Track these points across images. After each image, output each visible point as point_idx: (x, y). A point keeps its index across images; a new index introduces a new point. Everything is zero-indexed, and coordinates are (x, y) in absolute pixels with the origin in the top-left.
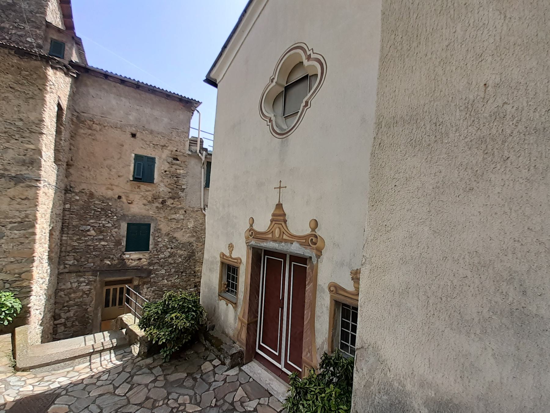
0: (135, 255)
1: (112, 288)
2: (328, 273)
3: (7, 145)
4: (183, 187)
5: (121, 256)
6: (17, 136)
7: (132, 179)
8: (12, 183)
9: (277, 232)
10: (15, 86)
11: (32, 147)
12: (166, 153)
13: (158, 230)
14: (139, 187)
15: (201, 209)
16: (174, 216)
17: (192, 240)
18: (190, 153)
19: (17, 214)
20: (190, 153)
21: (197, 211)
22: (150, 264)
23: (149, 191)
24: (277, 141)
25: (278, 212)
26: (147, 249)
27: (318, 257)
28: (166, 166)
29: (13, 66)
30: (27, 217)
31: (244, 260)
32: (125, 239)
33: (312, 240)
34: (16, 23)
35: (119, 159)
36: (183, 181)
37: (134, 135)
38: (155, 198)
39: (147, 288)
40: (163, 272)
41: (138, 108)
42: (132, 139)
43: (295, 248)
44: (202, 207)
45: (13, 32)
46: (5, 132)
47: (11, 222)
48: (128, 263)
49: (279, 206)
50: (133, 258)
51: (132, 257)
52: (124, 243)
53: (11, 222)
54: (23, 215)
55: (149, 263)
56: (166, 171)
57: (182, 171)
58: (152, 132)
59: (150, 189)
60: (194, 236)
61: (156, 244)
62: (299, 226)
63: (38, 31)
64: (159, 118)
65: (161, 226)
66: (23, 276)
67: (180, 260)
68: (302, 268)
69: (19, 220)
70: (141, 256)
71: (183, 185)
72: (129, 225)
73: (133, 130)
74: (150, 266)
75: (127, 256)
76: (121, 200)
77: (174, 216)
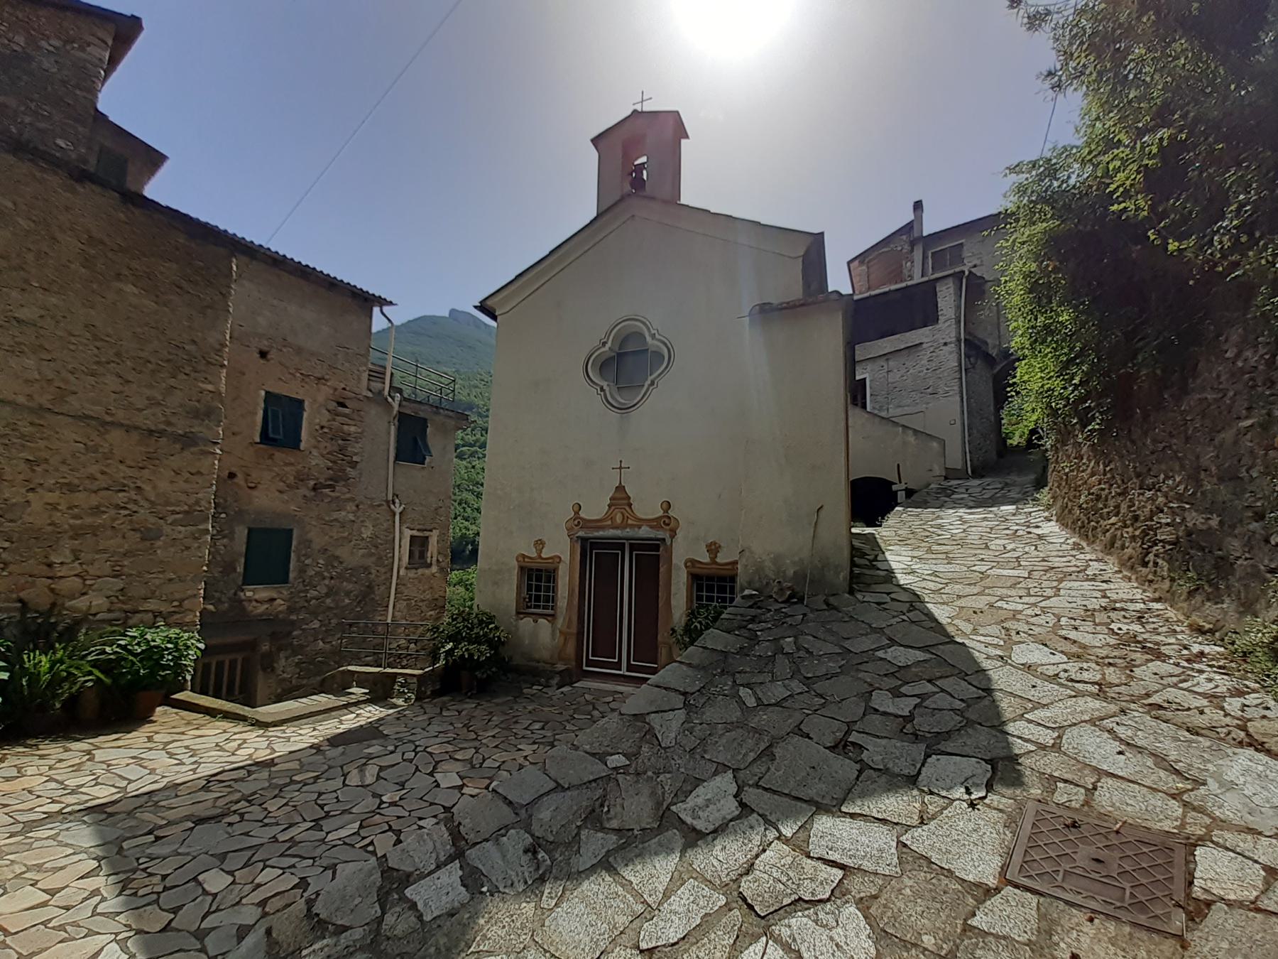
0: (263, 593)
1: (227, 659)
2: (684, 551)
3: (172, 382)
4: (355, 459)
5: (235, 594)
6: (188, 369)
7: (258, 440)
8: (178, 446)
9: (619, 519)
10: (184, 284)
11: (210, 387)
12: (325, 392)
13: (307, 543)
14: (271, 457)
15: (388, 502)
16: (335, 515)
17: (369, 561)
18: (370, 395)
19: (183, 497)
20: (370, 395)
21: (379, 506)
22: (291, 610)
23: (292, 464)
24: (614, 416)
25: (618, 495)
26: (286, 581)
27: (672, 537)
28: (324, 417)
29: (177, 249)
30: (197, 502)
31: (566, 557)
32: (243, 560)
33: (666, 521)
34: (32, 101)
35: (234, 399)
36: (354, 448)
37: (263, 354)
38: (301, 478)
39: (287, 658)
40: (316, 624)
41: (275, 302)
42: (262, 361)
43: (645, 532)
44: (390, 498)
45: (27, 120)
46: (168, 361)
47: (174, 512)
48: (250, 608)
49: (620, 488)
50: (258, 597)
51: (257, 597)
52: (240, 569)
53: (174, 512)
54: (191, 501)
55: (289, 608)
56: (322, 427)
57: (353, 429)
58: (299, 351)
59: (292, 460)
60: (372, 555)
61: (302, 570)
62: (646, 507)
63: (80, 129)
64: (306, 322)
65: (311, 535)
66: (186, 604)
67: (347, 601)
68: (650, 556)
69: (186, 508)
70: (275, 596)
71: (356, 454)
72: (250, 530)
73: (264, 345)
74: (292, 613)
75: (249, 594)
76: (236, 480)
77: (335, 515)
